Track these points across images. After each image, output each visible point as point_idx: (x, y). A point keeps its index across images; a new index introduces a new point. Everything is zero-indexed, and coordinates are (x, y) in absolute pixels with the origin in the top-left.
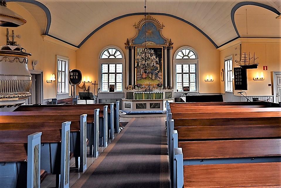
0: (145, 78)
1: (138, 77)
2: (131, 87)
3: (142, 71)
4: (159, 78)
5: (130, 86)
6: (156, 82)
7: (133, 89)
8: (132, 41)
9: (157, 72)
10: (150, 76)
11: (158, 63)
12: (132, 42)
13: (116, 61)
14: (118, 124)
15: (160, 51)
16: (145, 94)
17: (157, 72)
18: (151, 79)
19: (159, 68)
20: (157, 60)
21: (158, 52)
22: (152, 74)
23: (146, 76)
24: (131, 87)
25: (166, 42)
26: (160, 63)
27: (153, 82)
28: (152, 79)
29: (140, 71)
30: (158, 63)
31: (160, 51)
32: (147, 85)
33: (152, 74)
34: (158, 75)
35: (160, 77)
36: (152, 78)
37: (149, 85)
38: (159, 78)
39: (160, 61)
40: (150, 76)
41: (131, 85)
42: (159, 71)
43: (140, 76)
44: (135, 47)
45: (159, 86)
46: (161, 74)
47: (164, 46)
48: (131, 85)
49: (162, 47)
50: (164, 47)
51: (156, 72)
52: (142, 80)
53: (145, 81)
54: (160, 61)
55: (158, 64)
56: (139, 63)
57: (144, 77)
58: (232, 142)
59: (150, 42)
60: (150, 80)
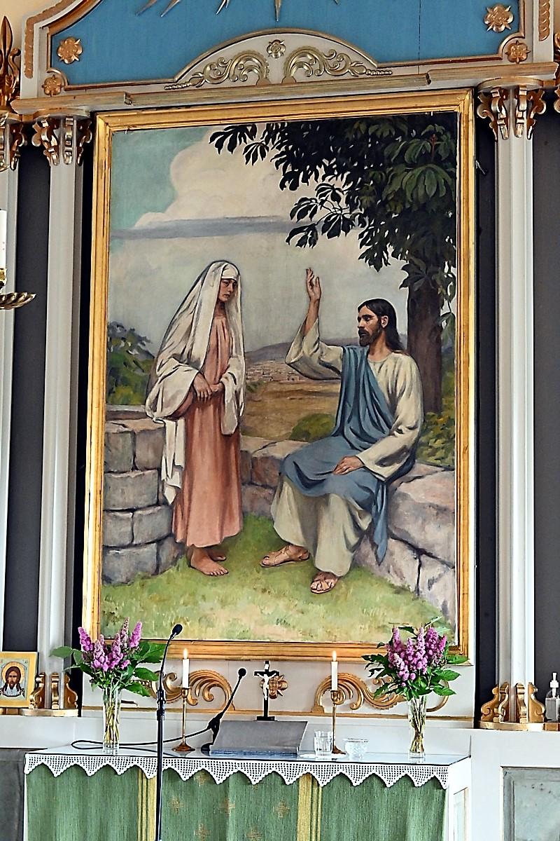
0: (213, 553)
1: (120, 531)
2: (28, 681)
3: (175, 450)
4: (420, 552)
5: (18, 658)
6: (364, 620)
7: (43, 703)
8: (57, 34)
9: (383, 462)
10: (288, 527)
11: (402, 327)
12: (54, 58)
13: (14, 676)
14: (339, 395)
15: (425, 158)
16: (174, 799)
17: (383, 462)
18: (298, 572)
19: (409, 410)
20: (391, 285)
21: (404, 179)
22: (313, 490)
23: (234, 528)
24: (28, 681)
25: (516, 26)
26: (424, 344)
27: (318, 609)
28: (317, 574)
29: (145, 454)
30: (402, 327)
31: (425, 158)
32: (243, 652)
33: (313, 490)
34: (403, 508)
35: (433, 535)
36: (306, 556)
37: (273, 662)
38: (420, 552)
39: (426, 297)
40: (288, 527)
41: (31, 645)
42: (408, 459)
43: (154, 523)
44: (87, 125)
45: (403, 672)
46: (436, 497)
47: (491, 76)
48: (31, 645)
49: (464, 106)
50: (480, 95)
51: (370, 456)
52: (178, 577)
53: (214, 591)
54: (426, 297)
55: (394, 345)
56: (118, 442)
57: (202, 530)
58: (31, 790)
59: (293, 42)
60: (281, 580)
